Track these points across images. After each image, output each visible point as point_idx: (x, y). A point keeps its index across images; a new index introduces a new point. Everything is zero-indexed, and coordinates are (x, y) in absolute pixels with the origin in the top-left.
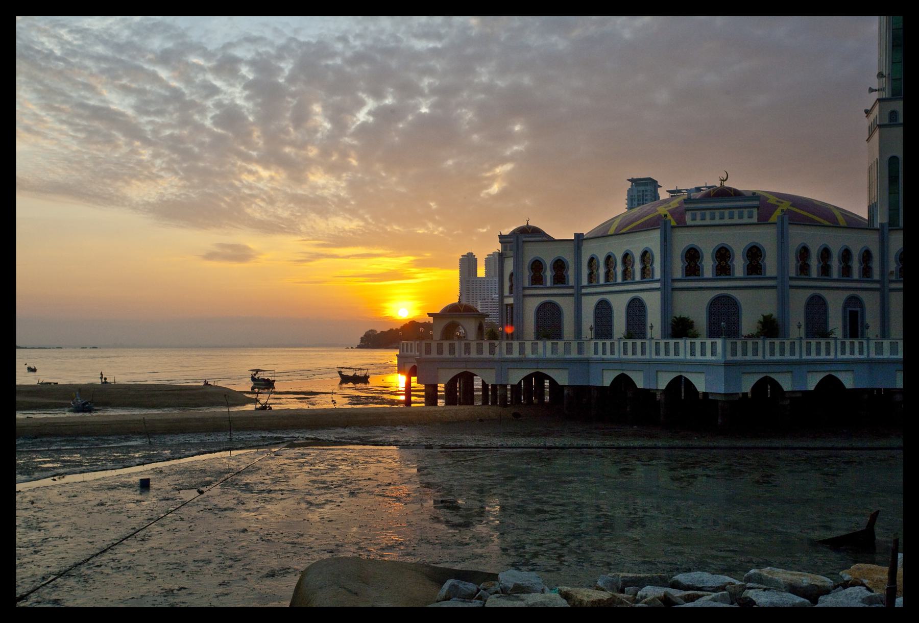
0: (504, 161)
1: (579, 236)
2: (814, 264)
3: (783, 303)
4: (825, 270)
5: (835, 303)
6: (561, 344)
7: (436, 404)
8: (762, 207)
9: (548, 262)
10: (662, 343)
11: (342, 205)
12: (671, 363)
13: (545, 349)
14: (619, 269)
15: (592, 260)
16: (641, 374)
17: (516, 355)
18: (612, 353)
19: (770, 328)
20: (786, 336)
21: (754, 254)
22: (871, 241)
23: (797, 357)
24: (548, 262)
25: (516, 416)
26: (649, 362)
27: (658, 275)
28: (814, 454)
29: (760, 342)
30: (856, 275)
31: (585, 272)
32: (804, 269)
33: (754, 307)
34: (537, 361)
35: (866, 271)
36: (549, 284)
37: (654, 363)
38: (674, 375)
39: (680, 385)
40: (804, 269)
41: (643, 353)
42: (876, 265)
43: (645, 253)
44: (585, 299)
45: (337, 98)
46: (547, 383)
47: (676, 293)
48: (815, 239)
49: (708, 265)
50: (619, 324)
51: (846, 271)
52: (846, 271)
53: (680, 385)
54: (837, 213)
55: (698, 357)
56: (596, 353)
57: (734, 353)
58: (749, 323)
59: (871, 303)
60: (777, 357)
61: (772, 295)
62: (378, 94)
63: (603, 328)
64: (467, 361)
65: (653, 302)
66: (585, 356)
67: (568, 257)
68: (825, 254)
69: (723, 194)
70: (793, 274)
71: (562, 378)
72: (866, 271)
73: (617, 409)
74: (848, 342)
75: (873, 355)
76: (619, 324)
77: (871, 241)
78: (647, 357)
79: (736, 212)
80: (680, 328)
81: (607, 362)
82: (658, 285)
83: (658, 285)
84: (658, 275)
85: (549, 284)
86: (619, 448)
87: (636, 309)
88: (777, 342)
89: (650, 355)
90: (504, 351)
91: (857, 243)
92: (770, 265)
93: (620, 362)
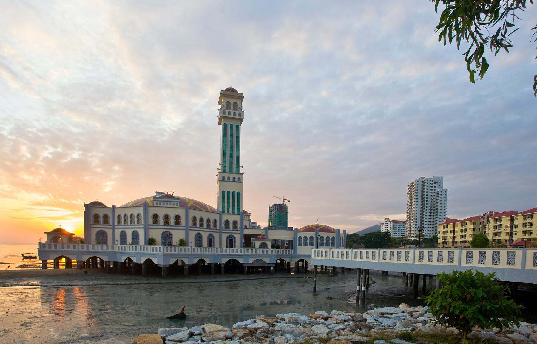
0: (111, 180)
1: (114, 207)
2: (198, 222)
3: (187, 235)
4: (202, 225)
5: (205, 236)
6: (254, 250)
7: (58, 268)
8: (182, 203)
9: (231, 221)
10: (120, 246)
11: (35, 189)
12: (125, 253)
13: (98, 248)
14: (136, 219)
15: (119, 216)
16: (135, 258)
17: (85, 249)
18: (125, 250)
19: (183, 243)
20: (188, 246)
21: (177, 218)
22: (217, 217)
23: (190, 253)
24: (231, 221)
25: (86, 272)
26: (138, 254)
27: (143, 223)
28: (192, 284)
29: (177, 248)
30: (198, 226)
31: (116, 220)
32: (194, 224)
33: (178, 235)
34: (95, 252)
35: (215, 226)
36: (101, 223)
37: (140, 254)
38: (176, 259)
39: (149, 262)
40: (194, 224)
41: (136, 250)
42: (218, 224)
43: (138, 215)
44: (116, 230)
45: (33, 145)
46: (98, 260)
47: (150, 230)
48: (199, 215)
49: (161, 220)
50: (129, 239)
51: (209, 226)
52: (209, 226)
53: (149, 262)
54: (208, 207)
55: (155, 252)
56: (119, 249)
57: (167, 251)
58: (176, 240)
59: (216, 236)
60: (183, 253)
61: (184, 232)
62: (55, 146)
63: (123, 241)
64: (62, 251)
65: (141, 232)
66: (115, 251)
67: (110, 214)
68: (202, 220)
69: (168, 196)
70: (191, 226)
71: (105, 259)
72: (215, 226)
73: (127, 269)
74: (243, 249)
75: (215, 253)
76: (129, 239)
77: (217, 217)
78: (137, 251)
79: (169, 203)
80: (151, 242)
81: (123, 253)
82: (143, 226)
83: (143, 226)
84: (143, 223)
85: (101, 223)
86: (89, 285)
87: (135, 235)
88: (155, 247)
89: (138, 251)
90: (80, 248)
91: (212, 217)
92: (183, 221)
93: (148, 254)
